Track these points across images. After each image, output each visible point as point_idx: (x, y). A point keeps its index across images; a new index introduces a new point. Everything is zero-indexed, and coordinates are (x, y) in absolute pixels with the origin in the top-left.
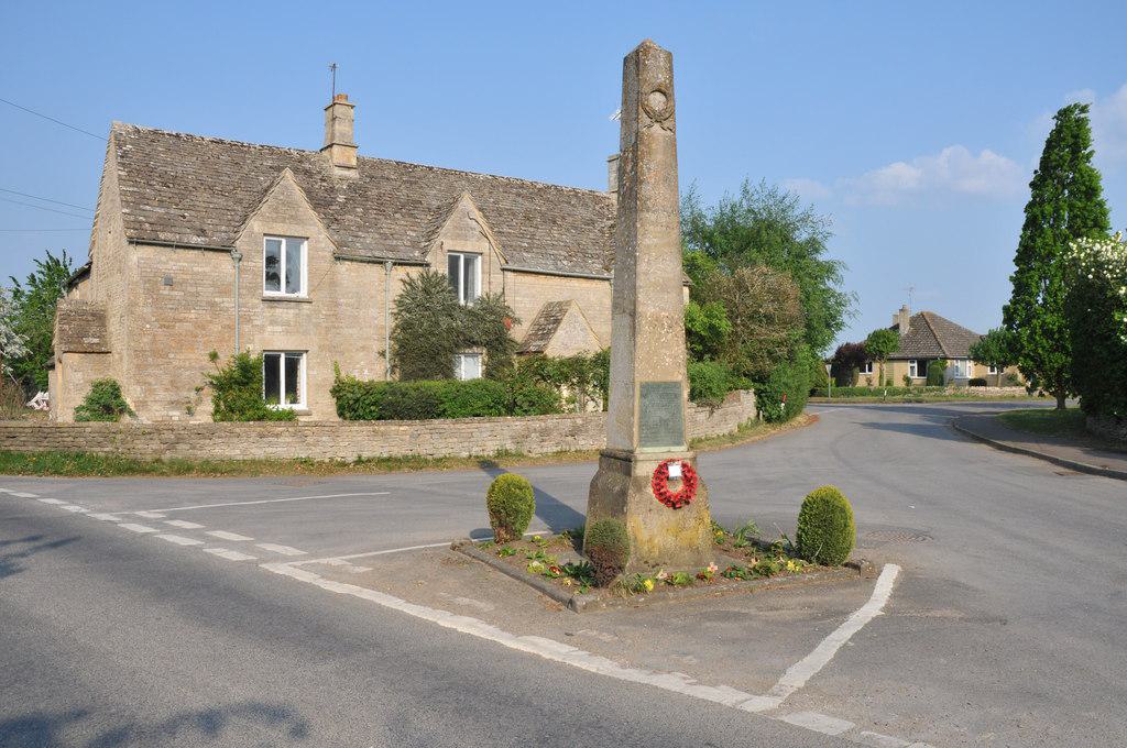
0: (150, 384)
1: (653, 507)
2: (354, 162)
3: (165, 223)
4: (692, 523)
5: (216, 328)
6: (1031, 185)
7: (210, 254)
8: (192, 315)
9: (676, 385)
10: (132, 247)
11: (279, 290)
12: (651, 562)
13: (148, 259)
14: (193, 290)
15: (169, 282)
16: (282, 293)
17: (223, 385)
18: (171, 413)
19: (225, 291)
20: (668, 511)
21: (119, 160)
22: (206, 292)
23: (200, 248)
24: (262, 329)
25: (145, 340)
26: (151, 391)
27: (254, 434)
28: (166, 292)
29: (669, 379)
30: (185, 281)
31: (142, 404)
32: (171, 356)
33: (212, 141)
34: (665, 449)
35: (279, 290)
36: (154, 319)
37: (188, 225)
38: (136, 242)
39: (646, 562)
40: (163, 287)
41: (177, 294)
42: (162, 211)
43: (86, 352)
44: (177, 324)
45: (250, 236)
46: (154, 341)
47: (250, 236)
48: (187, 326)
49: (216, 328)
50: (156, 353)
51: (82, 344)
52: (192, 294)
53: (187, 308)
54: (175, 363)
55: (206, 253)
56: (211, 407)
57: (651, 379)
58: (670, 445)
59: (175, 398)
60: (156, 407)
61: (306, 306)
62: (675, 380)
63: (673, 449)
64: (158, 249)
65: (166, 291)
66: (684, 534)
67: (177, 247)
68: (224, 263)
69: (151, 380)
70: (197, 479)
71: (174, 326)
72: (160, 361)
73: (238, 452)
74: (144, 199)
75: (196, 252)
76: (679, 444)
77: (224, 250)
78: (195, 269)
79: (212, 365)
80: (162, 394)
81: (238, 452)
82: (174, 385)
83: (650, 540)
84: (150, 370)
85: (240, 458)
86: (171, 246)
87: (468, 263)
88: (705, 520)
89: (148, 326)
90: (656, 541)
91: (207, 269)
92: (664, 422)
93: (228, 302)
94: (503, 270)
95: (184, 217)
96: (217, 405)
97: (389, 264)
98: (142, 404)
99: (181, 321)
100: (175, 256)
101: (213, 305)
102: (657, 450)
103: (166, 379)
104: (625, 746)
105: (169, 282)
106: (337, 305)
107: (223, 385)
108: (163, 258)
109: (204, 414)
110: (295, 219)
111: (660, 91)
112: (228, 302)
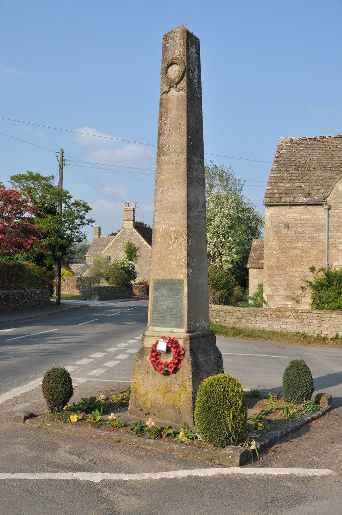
0: (275, 286)
1: (150, 371)
3: (287, 193)
4: (177, 388)
5: (314, 252)
7: (310, 208)
8: (300, 245)
9: (180, 282)
10: (266, 208)
12: (145, 411)
13: (276, 214)
14: (300, 230)
15: (287, 227)
17: (318, 287)
18: (287, 303)
20: (159, 377)
21: (276, 159)
22: (308, 231)
23: (304, 205)
25: (273, 260)
27: (275, 316)
28: (285, 232)
29: (173, 277)
30: (296, 225)
31: (271, 297)
32: (288, 269)
33: (336, 137)
34: (169, 329)
36: (278, 248)
37: (302, 191)
38: (269, 205)
39: (141, 410)
40: (283, 230)
41: (291, 233)
42: (290, 185)
43: (259, 268)
44: (291, 251)
45: (336, 194)
46: (278, 261)
47: (336, 194)
48: (297, 252)
49: (314, 252)
50: (279, 268)
51: (258, 263)
52: (299, 232)
53: (297, 241)
54: (290, 274)
55: (308, 207)
56: (310, 301)
57: (161, 277)
58: (173, 327)
59: (289, 294)
60: (279, 299)
62: (178, 278)
63: (176, 330)
64: (281, 207)
65: (285, 232)
66: (169, 395)
67: (291, 205)
68: (320, 213)
69: (276, 283)
70: (241, 340)
71: (289, 252)
72: (281, 272)
73: (267, 326)
74: (282, 179)
75: (302, 207)
78: (302, 217)
79: (311, 274)
80: (282, 292)
81: (267, 326)
82: (289, 286)
83: (146, 395)
84: (276, 278)
85: (268, 330)
86: (287, 205)
88: (187, 388)
89: (275, 252)
90: (149, 396)
91: (309, 217)
92: (170, 309)
95: (301, 187)
96: (315, 300)
98: (271, 297)
99: (293, 249)
100: (290, 211)
101: (312, 238)
102: (163, 329)
103: (284, 283)
104: (5, 514)
105: (287, 227)
107: (318, 287)
108: (284, 213)
109: (306, 302)
111: (168, 67)
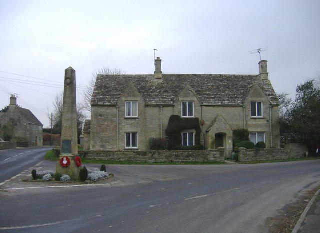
2: (161, 77)
3: (101, 100)
6: (161, 61)
8: (106, 123)
9: (223, 147)
11: (256, 116)
15: (101, 115)
16: (131, 116)
19: (115, 117)
24: (125, 126)
26: (96, 143)
35: (256, 116)
61: (137, 120)
68: (115, 110)
74: (98, 94)
76: (70, 153)
77: (114, 106)
80: (98, 144)
82: (102, 141)
87: (259, 104)
93: (115, 119)
94: (202, 106)
97: (162, 107)
105: (101, 115)
106: (147, 119)
110: (134, 96)
112: (115, 119)
